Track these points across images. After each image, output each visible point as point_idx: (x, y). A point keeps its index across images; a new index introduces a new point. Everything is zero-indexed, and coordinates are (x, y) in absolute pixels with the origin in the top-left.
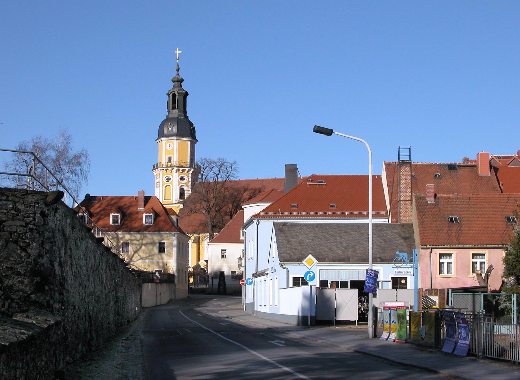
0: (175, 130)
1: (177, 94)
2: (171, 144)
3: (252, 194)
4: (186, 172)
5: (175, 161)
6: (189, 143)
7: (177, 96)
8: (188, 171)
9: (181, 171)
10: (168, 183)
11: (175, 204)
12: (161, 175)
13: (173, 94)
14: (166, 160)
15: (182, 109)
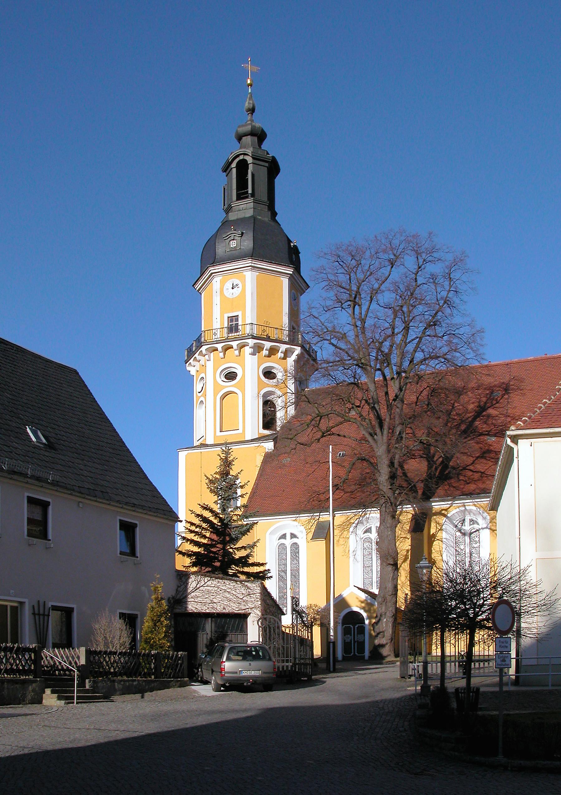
0: (248, 243)
1: (249, 160)
2: (236, 282)
3: (484, 399)
4: (280, 355)
5: (248, 321)
6: (285, 282)
7: (251, 167)
8: (287, 354)
9: (265, 352)
10: (230, 386)
11: (252, 440)
12: (210, 365)
13: (240, 161)
14: (222, 322)
15: (265, 198)
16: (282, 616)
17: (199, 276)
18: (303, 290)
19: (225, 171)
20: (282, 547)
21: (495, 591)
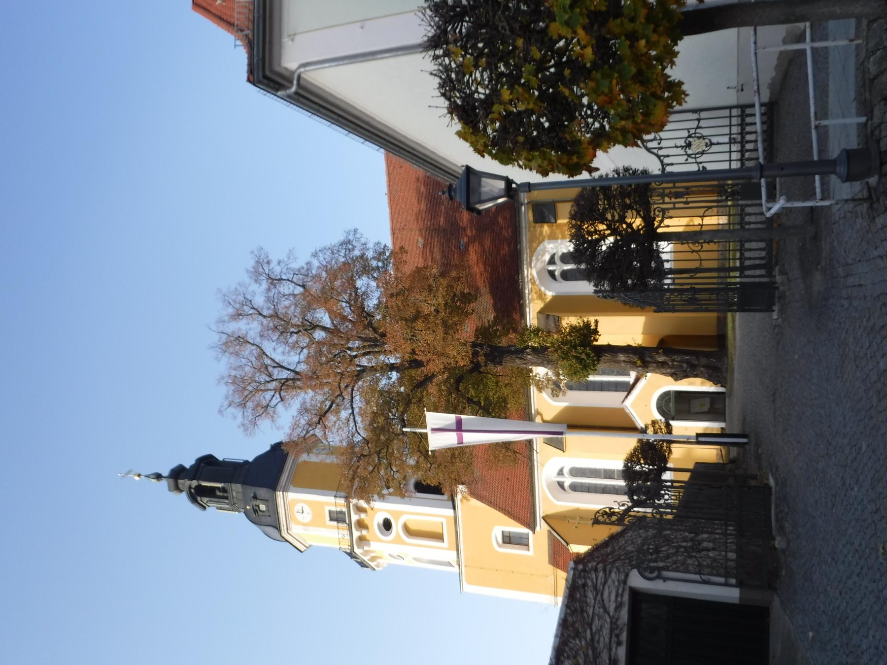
10: (397, 527)
16: (567, 176)
17: (288, 543)
18: (316, 441)
19: (205, 508)
20: (575, 488)
21: (661, 514)
